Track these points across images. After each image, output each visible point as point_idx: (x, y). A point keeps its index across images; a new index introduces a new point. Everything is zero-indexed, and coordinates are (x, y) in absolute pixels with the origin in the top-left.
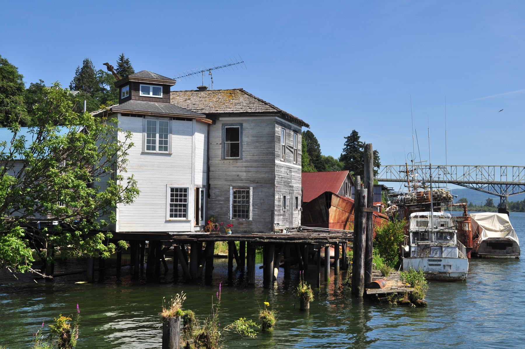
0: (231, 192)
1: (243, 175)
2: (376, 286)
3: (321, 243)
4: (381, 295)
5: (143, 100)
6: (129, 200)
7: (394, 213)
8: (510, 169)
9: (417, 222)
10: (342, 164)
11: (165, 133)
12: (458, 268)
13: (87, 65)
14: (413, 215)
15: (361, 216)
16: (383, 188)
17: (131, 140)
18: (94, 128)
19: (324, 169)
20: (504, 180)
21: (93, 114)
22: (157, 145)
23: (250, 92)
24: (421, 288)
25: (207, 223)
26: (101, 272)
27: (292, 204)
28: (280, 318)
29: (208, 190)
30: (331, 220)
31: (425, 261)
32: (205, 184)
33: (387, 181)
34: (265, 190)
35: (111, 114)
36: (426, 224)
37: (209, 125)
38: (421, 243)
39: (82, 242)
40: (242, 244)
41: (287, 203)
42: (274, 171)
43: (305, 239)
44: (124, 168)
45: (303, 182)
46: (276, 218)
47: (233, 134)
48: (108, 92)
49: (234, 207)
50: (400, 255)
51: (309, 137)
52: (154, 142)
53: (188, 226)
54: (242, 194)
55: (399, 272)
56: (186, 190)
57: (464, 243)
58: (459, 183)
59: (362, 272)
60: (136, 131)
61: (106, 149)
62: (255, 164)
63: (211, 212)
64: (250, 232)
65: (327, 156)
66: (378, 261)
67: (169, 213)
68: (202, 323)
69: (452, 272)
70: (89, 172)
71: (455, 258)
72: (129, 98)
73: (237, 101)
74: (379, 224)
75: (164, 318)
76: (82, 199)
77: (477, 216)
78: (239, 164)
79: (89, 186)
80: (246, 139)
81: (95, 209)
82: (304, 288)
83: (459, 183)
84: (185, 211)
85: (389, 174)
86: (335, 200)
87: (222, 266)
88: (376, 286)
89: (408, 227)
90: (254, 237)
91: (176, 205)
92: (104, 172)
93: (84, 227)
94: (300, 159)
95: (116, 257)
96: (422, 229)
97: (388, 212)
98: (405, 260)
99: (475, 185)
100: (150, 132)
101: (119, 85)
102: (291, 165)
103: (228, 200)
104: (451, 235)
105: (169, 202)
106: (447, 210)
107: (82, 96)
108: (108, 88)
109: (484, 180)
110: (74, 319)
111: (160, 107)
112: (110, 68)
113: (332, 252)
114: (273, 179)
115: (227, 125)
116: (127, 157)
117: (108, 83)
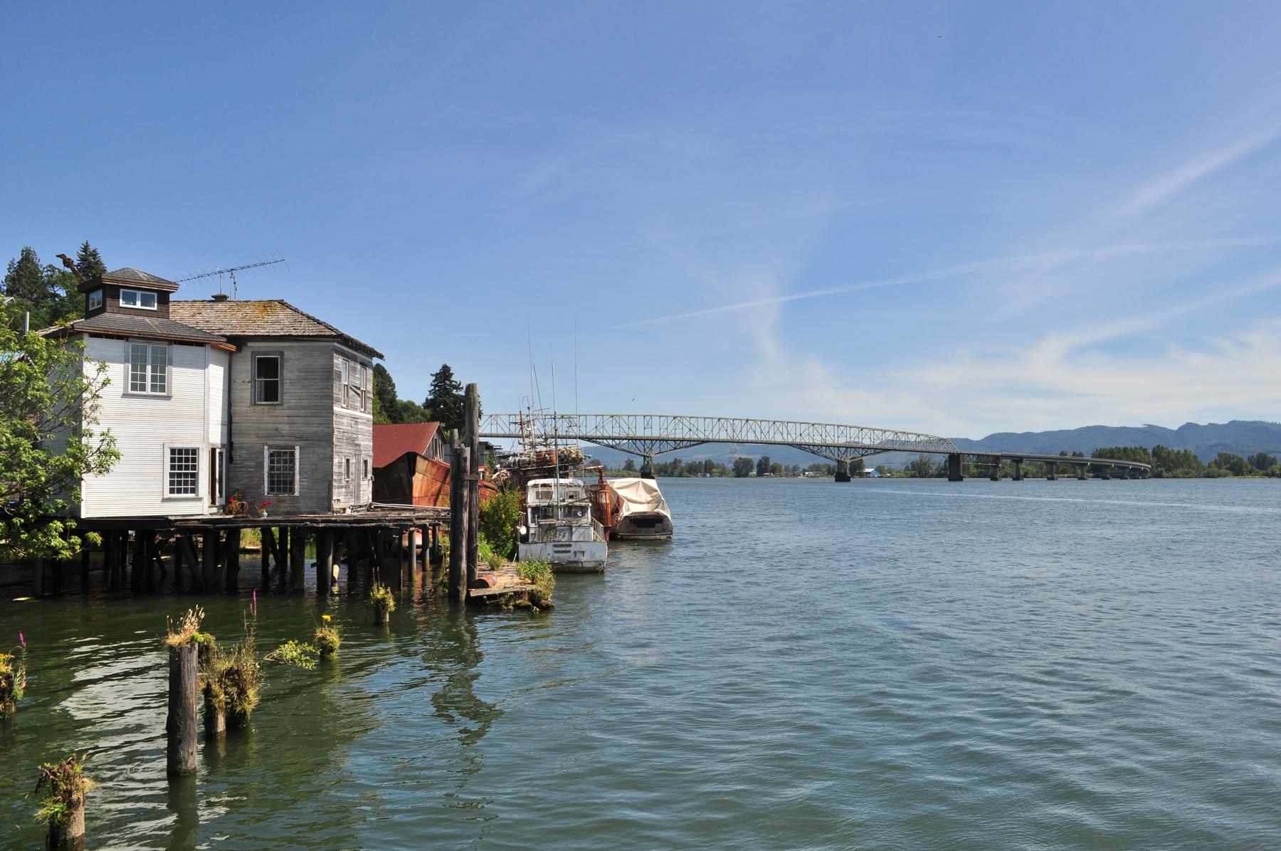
0: (266, 454)
1: (285, 429)
2: (484, 584)
3: (403, 527)
4: (491, 597)
5: (128, 312)
6: (103, 469)
7: (505, 482)
8: (655, 420)
9: (538, 493)
10: (427, 412)
11: (161, 365)
12: (593, 555)
13: (27, 257)
14: (531, 483)
15: (462, 486)
16: (488, 447)
17: (105, 376)
18: (45, 355)
19: (402, 420)
20: (648, 434)
21: (40, 333)
22: (149, 383)
23: (294, 306)
24: (545, 584)
25: (228, 501)
26: (55, 581)
27: (359, 470)
28: (346, 639)
29: (230, 451)
30: (416, 493)
31: (550, 546)
32: (225, 442)
33: (491, 436)
34: (319, 450)
35: (71, 335)
36: (548, 495)
37: (231, 353)
38: (543, 522)
39: (24, 536)
40: (283, 531)
41: (352, 469)
42: (331, 422)
43: (379, 520)
44: (95, 419)
45: (376, 438)
46: (335, 491)
47: (268, 368)
48: (62, 299)
49: (271, 476)
50: (515, 539)
51: (380, 373)
52: (143, 378)
53: (199, 506)
54: (282, 457)
55: (514, 564)
56: (194, 451)
57: (601, 520)
58: (590, 439)
59: (464, 565)
60: (113, 361)
61: (65, 389)
62: (303, 412)
63: (235, 485)
64: (295, 513)
65: (405, 400)
66: (484, 549)
67: (167, 487)
68: (229, 653)
69: (587, 560)
70: (36, 425)
71: (589, 542)
72: (102, 310)
73: (274, 319)
74: (484, 496)
75: (171, 648)
76: (25, 466)
77: (616, 484)
78: (279, 412)
79: (35, 446)
80: (289, 375)
81: (47, 482)
82: (380, 592)
83: (590, 439)
84: (193, 483)
85: (494, 427)
86: (421, 464)
87: (253, 566)
88: (484, 584)
89: (525, 501)
90: (303, 521)
91: (179, 475)
92: (62, 424)
93: (27, 513)
94: (370, 405)
95: (80, 558)
96: (544, 503)
97: (495, 481)
98: (522, 547)
99: (610, 442)
100: (137, 362)
101: (87, 289)
102: (357, 413)
103: (261, 465)
104: (583, 509)
105: (168, 470)
106: (575, 476)
107: (19, 305)
108: (62, 293)
109: (623, 435)
110: (17, 653)
111: (153, 325)
112: (67, 262)
113: (418, 540)
114: (331, 435)
115: (259, 353)
116: (99, 401)
117: (65, 287)
